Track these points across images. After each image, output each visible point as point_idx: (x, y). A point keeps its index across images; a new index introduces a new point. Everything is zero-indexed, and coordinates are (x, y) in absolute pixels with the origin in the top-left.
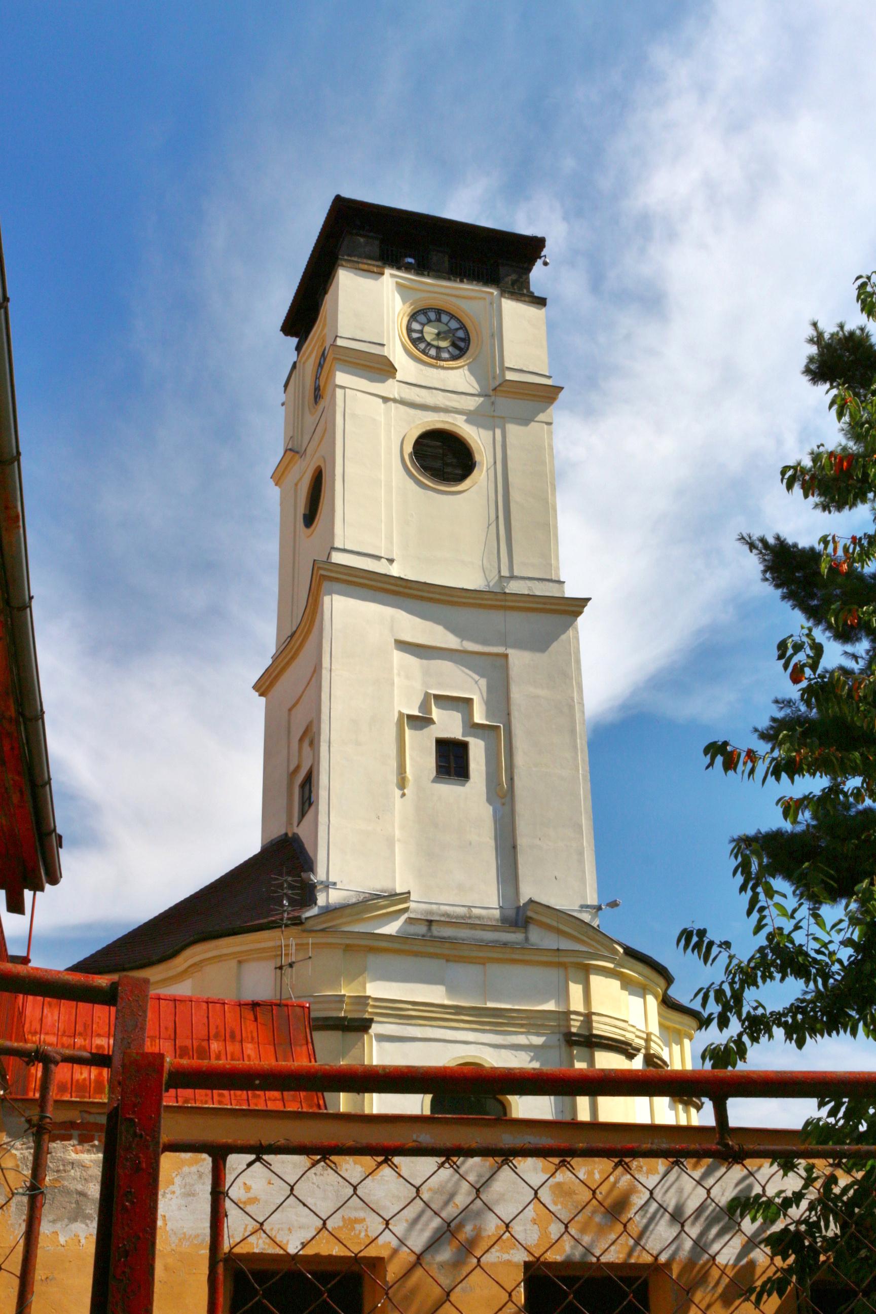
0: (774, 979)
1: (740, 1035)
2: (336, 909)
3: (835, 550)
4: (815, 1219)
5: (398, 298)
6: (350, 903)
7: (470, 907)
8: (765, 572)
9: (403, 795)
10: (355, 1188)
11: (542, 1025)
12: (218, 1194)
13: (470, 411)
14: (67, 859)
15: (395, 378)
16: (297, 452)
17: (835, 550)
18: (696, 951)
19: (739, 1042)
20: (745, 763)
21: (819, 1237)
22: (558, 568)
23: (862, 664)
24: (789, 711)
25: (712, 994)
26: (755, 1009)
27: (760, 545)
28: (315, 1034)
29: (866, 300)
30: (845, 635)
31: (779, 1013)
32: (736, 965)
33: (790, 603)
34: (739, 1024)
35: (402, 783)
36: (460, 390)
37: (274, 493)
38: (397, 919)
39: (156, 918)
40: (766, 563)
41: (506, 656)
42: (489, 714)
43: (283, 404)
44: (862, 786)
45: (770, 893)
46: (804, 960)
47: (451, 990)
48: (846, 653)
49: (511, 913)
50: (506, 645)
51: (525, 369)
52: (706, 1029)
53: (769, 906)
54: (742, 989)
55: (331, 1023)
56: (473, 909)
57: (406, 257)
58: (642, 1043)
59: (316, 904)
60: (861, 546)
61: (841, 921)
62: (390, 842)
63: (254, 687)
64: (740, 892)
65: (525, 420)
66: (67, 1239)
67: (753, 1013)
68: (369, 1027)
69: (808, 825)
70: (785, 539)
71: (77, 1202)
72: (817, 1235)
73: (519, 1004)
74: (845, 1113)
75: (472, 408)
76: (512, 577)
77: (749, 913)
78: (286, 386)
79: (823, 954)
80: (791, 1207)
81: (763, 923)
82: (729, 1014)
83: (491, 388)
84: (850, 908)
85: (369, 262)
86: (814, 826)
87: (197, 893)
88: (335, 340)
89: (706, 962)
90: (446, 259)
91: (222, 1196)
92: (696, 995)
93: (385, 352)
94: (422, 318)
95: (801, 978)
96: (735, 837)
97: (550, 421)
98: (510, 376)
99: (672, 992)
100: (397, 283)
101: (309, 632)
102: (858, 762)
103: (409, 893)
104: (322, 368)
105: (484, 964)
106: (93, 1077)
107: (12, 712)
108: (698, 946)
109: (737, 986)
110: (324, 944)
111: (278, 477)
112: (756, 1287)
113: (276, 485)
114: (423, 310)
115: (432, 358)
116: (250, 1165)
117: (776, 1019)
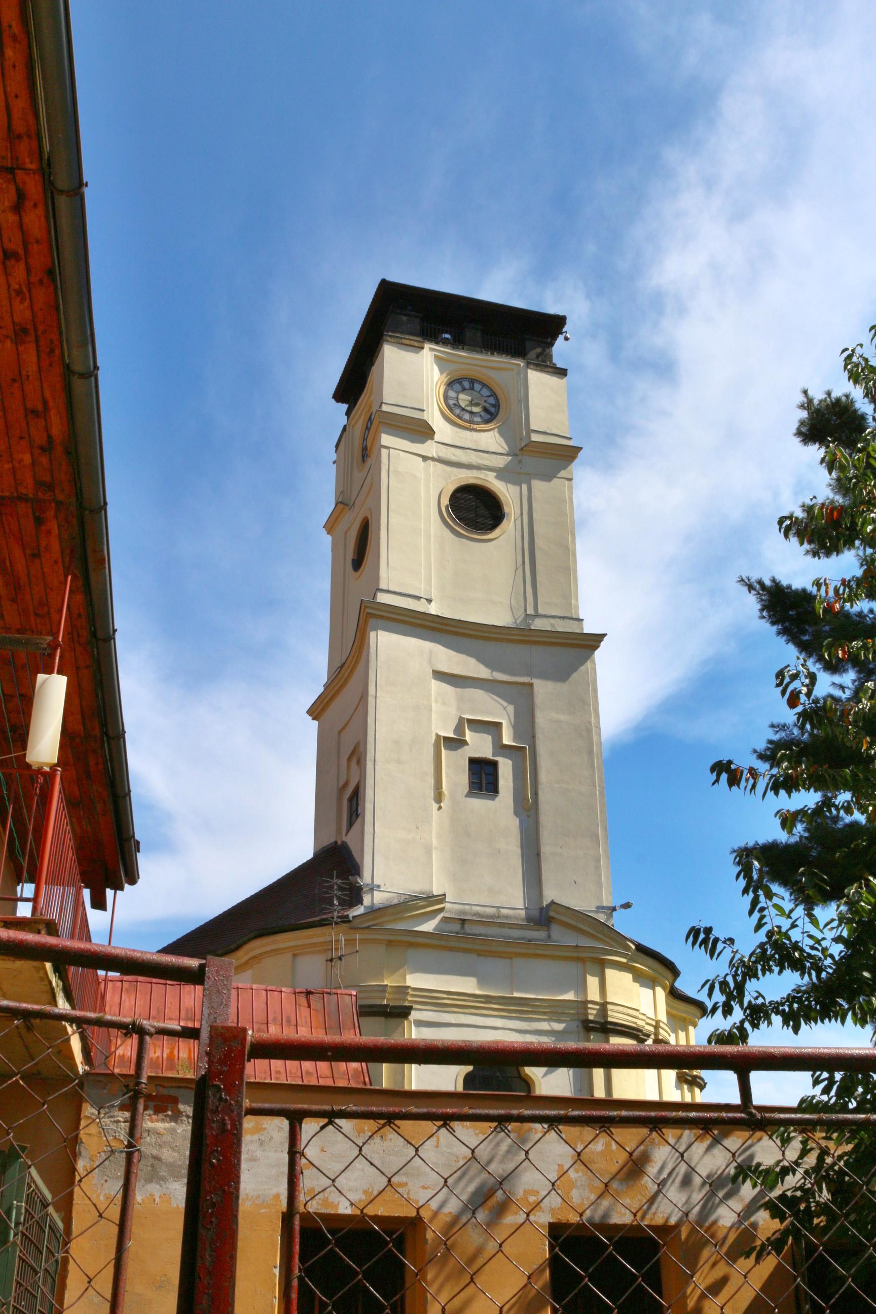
0: (773, 972)
1: (742, 1022)
2: (380, 909)
3: (827, 592)
4: (809, 1186)
5: (436, 369)
6: (392, 904)
7: (498, 908)
8: (762, 610)
9: (440, 808)
10: (417, 1150)
11: (563, 1013)
12: (294, 1153)
13: (500, 468)
14: (144, 862)
15: (433, 439)
16: (347, 505)
17: (827, 592)
18: (703, 947)
19: (741, 1028)
20: (747, 780)
21: (813, 1202)
22: (577, 607)
23: (848, 693)
24: (783, 734)
25: (717, 986)
26: (756, 998)
27: (758, 587)
28: (362, 1019)
29: (852, 370)
30: (833, 667)
31: (777, 1002)
32: (739, 959)
33: (785, 638)
34: (742, 1012)
35: (439, 798)
36: (491, 450)
37: (327, 540)
38: (434, 918)
39: (220, 915)
40: (764, 603)
41: (531, 685)
42: (516, 736)
43: (334, 463)
44: (852, 800)
45: (769, 895)
46: (799, 955)
47: (481, 982)
48: (834, 684)
49: (536, 913)
50: (530, 675)
51: (548, 431)
52: (712, 1017)
53: (768, 908)
54: (744, 981)
55: (375, 1010)
56: (501, 910)
57: (443, 333)
58: (652, 1029)
59: (362, 904)
60: (850, 588)
61: (833, 920)
62: (428, 850)
63: (308, 712)
64: (743, 894)
65: (548, 477)
66: (144, 1197)
67: (753, 1002)
68: (409, 1014)
69: (801, 837)
70: (780, 582)
71: (152, 1166)
72: (811, 1200)
73: (541, 995)
74: (837, 1091)
75: (501, 466)
76: (537, 615)
77: (751, 913)
78: (337, 446)
79: (817, 949)
80: (788, 1175)
81: (763, 922)
82: (732, 1003)
83: (519, 448)
84: (840, 909)
85: (411, 337)
86: (806, 838)
87: (256, 894)
88: (381, 406)
89: (712, 957)
90: (479, 334)
91: (298, 1155)
92: (703, 986)
93: (425, 416)
94: (457, 387)
95: (797, 971)
96: (736, 848)
97: (570, 477)
98: (535, 438)
99: (680, 984)
100: (435, 356)
101: (357, 662)
102: (848, 778)
103: (445, 895)
104: (369, 430)
105: (511, 958)
106: (165, 1055)
107: (97, 733)
108: (705, 942)
109: (739, 978)
110: (371, 940)
111: (330, 526)
112: (756, 1247)
113: (328, 533)
114: (458, 379)
115: (466, 421)
116: (322, 1128)
117: (774, 1007)
